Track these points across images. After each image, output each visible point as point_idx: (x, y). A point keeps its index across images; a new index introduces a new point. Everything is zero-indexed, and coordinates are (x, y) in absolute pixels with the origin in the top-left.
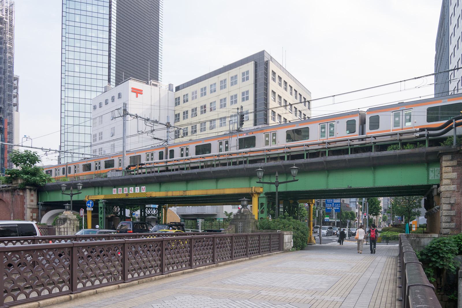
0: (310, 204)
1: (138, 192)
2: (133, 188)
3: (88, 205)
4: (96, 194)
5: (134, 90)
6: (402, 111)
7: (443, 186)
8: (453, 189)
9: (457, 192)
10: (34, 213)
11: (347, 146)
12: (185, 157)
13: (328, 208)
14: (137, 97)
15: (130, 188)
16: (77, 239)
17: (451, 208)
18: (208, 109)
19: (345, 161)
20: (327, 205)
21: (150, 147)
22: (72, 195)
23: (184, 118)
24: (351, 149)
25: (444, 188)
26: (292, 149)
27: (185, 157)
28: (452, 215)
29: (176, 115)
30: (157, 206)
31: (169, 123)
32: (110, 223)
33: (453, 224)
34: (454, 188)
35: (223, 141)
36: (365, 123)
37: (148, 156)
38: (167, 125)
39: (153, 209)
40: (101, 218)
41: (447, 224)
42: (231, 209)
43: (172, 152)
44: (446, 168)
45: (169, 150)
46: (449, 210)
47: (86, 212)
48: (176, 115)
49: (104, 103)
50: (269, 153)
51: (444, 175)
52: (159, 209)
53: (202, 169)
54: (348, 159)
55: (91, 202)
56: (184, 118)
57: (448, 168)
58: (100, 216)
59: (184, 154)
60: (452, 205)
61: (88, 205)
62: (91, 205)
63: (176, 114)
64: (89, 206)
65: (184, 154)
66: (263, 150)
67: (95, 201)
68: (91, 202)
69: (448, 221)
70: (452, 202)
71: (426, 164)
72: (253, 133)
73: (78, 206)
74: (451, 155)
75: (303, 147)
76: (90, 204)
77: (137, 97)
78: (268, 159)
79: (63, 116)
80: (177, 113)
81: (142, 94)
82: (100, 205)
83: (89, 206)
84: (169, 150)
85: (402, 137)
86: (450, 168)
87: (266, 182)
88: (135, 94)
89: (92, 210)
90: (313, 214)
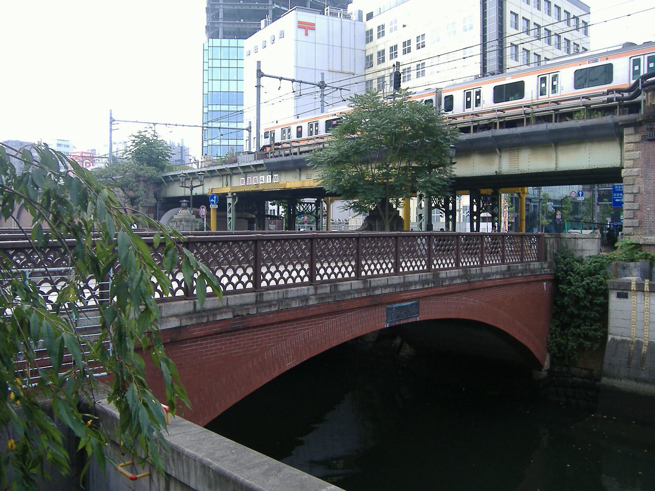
0: (521, 195)
1: (270, 182)
2: (263, 177)
3: (212, 200)
4: (225, 186)
5: (302, 25)
6: (643, 56)
7: (625, 170)
8: (636, 174)
9: (641, 177)
10: (150, 213)
11: (522, 114)
12: (314, 136)
13: (617, 200)
14: (306, 34)
15: (261, 177)
16: (190, 245)
17: (634, 200)
18: (413, 46)
19: (517, 136)
20: (615, 194)
21: (461, 81)
22: (192, 188)
23: (379, 63)
24: (556, 115)
25: (626, 171)
26: (508, 112)
27: (314, 136)
28: (635, 208)
29: (367, 57)
30: (313, 200)
31: (323, 82)
32: (622, 249)
33: (636, 220)
34: (637, 172)
35: (642, 57)
36: (441, 105)
37: (543, 80)
38: (321, 84)
39: (307, 205)
40: (230, 218)
41: (630, 221)
42: (619, 200)
43: (450, 99)
44: (628, 145)
45: (444, 95)
46: (632, 202)
47: (208, 209)
48: (367, 57)
49: (260, 47)
50: (476, 118)
51: (626, 155)
52: (318, 204)
53: (475, 134)
54: (522, 134)
55: (215, 197)
56: (379, 63)
57: (630, 144)
58: (229, 215)
59: (314, 132)
60: (635, 194)
61: (212, 200)
62: (215, 201)
63: (367, 55)
64: (213, 203)
65: (314, 132)
66: (494, 111)
67: (220, 195)
68: (215, 197)
69: (631, 217)
70: (635, 191)
71: (298, 170)
72: (607, 59)
73: (201, 201)
74: (633, 128)
75: (579, 100)
76: (214, 199)
77: (306, 34)
78: (475, 127)
79: (206, 68)
80: (368, 53)
81: (314, 29)
82: (229, 201)
83: (213, 203)
84: (444, 95)
85: (559, 106)
86: (633, 144)
87: (196, 185)
88: (304, 30)
89: (217, 207)
90: (526, 210)
